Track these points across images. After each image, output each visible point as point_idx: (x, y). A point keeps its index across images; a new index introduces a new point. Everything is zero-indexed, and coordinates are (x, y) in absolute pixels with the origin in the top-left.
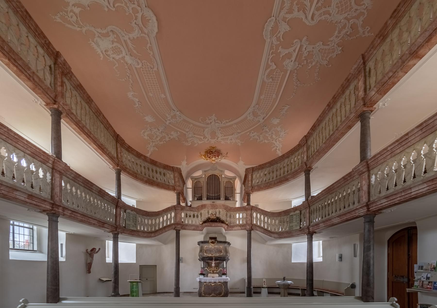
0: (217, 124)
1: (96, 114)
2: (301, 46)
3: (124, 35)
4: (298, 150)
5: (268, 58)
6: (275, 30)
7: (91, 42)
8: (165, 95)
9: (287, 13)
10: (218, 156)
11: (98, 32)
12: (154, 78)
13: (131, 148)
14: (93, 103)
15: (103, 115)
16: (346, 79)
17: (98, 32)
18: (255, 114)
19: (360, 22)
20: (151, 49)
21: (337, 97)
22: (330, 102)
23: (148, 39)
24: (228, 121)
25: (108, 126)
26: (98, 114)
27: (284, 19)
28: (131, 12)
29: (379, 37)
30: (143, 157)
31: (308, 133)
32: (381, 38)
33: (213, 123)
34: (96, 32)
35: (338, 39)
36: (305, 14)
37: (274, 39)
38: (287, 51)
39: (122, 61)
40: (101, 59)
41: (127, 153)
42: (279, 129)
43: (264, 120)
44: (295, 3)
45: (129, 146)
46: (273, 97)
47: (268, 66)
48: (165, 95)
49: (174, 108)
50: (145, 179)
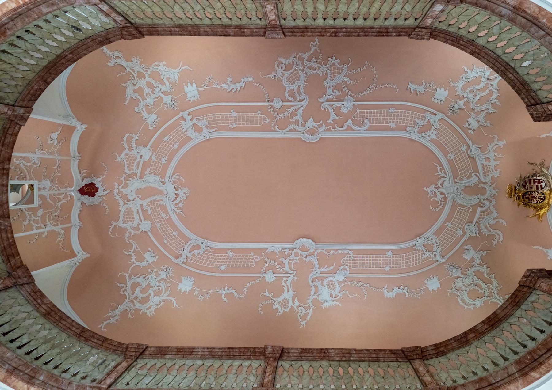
0: (446, 184)
1: (344, 359)
2: (328, 101)
3: (316, 272)
4: (446, 32)
5: (339, 131)
6: (312, 132)
7: (323, 306)
8: (388, 251)
9: (298, 125)
10: (539, 182)
11: (314, 295)
12: (209, 264)
13: (441, 343)
14: (331, 351)
15: (355, 350)
16: (294, 36)
17: (314, 295)
18: (424, 130)
19: (305, 56)
20: (328, 251)
21: (317, 31)
22: (331, 36)
23: (320, 251)
24: (439, 168)
25: (374, 355)
26: (348, 355)
27: (303, 125)
28: (297, 258)
29: (244, 32)
30: (472, 335)
31: (400, 35)
32: (242, 30)
33: (443, 191)
34: (314, 297)
35: (321, 66)
36: (299, 108)
37: (320, 130)
38: (332, 114)
39: (343, 285)
40: (340, 305)
41: (442, 359)
42: (460, 84)
43: (437, 113)
44: (291, 120)
45: (435, 345)
46: (393, 111)
47: (350, 129)
48: (388, 251)
49: (411, 244)
50: (513, 369)
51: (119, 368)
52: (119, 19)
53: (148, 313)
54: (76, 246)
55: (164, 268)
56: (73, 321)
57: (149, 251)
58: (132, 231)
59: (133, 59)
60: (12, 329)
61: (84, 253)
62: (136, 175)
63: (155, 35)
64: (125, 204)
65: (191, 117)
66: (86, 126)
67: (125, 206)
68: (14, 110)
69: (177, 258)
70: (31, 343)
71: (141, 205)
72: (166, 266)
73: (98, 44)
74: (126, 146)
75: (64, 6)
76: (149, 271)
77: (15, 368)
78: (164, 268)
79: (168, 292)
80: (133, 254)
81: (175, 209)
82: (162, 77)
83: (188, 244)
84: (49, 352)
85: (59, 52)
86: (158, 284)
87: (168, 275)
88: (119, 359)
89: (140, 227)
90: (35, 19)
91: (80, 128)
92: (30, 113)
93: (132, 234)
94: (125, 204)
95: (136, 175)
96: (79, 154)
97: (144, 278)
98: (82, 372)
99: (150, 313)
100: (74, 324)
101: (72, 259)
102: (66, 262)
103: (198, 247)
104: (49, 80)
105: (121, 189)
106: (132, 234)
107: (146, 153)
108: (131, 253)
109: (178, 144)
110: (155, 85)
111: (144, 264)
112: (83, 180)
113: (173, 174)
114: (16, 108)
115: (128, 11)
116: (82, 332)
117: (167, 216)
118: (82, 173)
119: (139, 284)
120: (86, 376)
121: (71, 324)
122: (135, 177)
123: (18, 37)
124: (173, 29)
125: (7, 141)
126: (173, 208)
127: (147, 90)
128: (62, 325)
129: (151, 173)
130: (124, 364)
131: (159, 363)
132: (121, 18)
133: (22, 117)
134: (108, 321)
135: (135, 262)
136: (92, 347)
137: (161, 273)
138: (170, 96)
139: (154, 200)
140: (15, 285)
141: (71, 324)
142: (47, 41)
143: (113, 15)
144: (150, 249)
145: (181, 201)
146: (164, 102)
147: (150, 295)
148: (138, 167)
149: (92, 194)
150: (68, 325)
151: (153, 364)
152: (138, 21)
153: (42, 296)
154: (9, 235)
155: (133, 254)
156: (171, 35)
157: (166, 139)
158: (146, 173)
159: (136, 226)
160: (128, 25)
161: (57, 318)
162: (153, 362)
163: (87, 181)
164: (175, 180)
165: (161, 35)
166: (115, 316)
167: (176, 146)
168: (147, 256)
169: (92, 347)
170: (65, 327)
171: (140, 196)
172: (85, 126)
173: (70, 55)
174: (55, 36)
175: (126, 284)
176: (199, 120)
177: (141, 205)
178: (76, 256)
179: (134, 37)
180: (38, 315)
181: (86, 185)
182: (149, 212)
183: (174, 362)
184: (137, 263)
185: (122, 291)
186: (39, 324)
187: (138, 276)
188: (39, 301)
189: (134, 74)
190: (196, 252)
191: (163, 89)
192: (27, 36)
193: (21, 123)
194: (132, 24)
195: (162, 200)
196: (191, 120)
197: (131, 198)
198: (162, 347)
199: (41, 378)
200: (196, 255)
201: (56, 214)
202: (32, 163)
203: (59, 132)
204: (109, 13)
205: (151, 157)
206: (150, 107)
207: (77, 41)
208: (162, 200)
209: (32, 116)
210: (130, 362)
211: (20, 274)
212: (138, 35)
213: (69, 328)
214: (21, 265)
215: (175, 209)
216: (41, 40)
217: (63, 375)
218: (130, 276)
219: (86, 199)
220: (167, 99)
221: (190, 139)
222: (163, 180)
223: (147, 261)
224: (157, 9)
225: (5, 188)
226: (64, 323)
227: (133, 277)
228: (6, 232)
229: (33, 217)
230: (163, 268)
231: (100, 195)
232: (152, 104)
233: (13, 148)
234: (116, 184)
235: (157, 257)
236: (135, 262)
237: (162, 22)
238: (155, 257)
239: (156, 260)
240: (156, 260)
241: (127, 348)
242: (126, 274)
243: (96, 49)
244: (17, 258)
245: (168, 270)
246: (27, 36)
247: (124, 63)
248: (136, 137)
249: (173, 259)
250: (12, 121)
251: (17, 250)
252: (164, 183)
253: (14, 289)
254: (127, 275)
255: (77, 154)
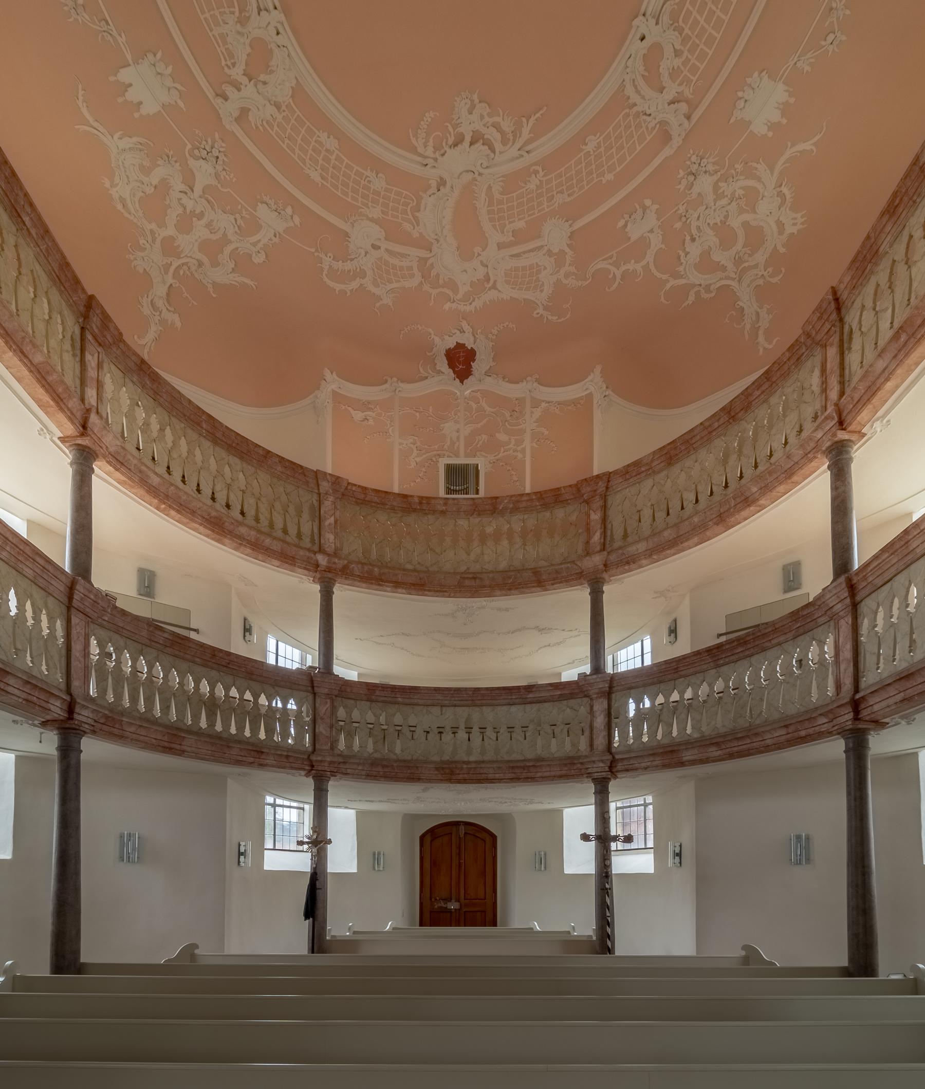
51: (829, 366)
52: (91, 360)
53: (794, 230)
54: (573, 392)
55: (684, 182)
56: (701, 424)
57: (626, 225)
58: (563, 271)
59: (141, 271)
60: (666, 509)
61: (590, 378)
62: (423, 261)
63: (73, 272)
64: (494, 287)
65: (229, 90)
66: (327, 373)
67: (499, 286)
68: (326, 494)
69: (666, 137)
70: (700, 489)
71: (500, 246)
72: (682, 173)
73: (160, 383)
74: (354, 285)
75: (134, 457)
76: (678, 225)
77: (720, 516)
78: (684, 182)
79: (762, 168)
80: (624, 268)
81: (518, 144)
82: (150, 190)
83: (635, 98)
84: (727, 471)
85: (207, 444)
86: (724, 202)
87: (711, 168)
88: (817, 360)
89: (555, 250)
90: (177, 487)
91: (332, 383)
92: (325, 474)
93: (573, 269)
94: (494, 287)
95: (423, 261)
96: (386, 382)
97: (693, 240)
98: (788, 432)
99: (794, 222)
100: (707, 424)
101: (595, 402)
102: (597, 415)
103: (653, 57)
104: (261, 452)
105: (460, 296)
106: (573, 269)
107: (364, 234)
108: (618, 274)
109: (323, 136)
110: (180, 211)
111: (656, 242)
112: (440, 372)
113: (414, 150)
114: (321, 491)
115: (67, 351)
116: (729, 412)
117: (536, 173)
118: (426, 375)
119: (706, 254)
120: (801, 426)
121: (706, 428)
122: (430, 262)
123: (213, 499)
124: (33, 232)
125: (376, 499)
126: (513, 151)
127: (200, 231)
128: (699, 443)
129: (417, 219)
130: (832, 352)
131: (881, 276)
132: (88, 357)
133: (333, 483)
134: (761, 332)
135: (643, 263)
136: (766, 401)
137: (696, 190)
138: (192, 163)
139: (489, 212)
140: (604, 498)
141: (706, 428)
142: (200, 464)
143: (92, 373)
144: (621, 223)
145: (496, 126)
146: (214, 182)
147: (746, 225)
148: (402, 255)
149: (471, 355)
150: (706, 432)
151: (872, 292)
152: (70, 320)
153: (637, 464)
154: (525, 498)
155: (624, 268)
156: (47, 231)
157: (315, 175)
158: (416, 235)
159: (552, 259)
160: (90, 337)
161: (683, 448)
162: (870, 289)
163: (443, 364)
164: (431, 144)
165: (64, 257)
166: (758, 314)
167: (331, 143)
168: (635, 231)
169: (764, 402)
170: (705, 439)
171: (477, 249)
172: (328, 375)
173: (204, 426)
174: (185, 454)
175: (694, 286)
176: (232, 56)
177: (500, 246)
178: (590, 396)
179: (106, 318)
180: (664, 473)
181: (451, 365)
182: (521, 224)
183: (905, 238)
184: (650, 258)
185: (705, 296)
186: (680, 474)
187: (682, 254)
188: (643, 469)
189: (175, 265)
190: (665, 66)
191: (178, 185)
192: (207, 491)
193: (345, 484)
194: (83, 329)
195: (490, 188)
196: (238, 87)
197: (481, 272)
198: (859, 252)
199: (754, 489)
200: (677, 62)
201: (507, 415)
202: (414, 448)
203: (350, 409)
204: (95, 383)
205: (372, 220)
206: (239, 221)
207: (173, 419)
208: (490, 188)
209: (329, 471)
210: (836, 339)
211: (589, 489)
212: (98, 312)
213: (710, 433)
214: (577, 487)
215: (518, 144)
216: (202, 472)
217: (773, 460)
218: (676, 276)
219: (478, 367)
220: (204, 173)
221: (298, 91)
222: (434, 184)
223: (651, 231)
224: (26, 293)
225: (450, 502)
226: (698, 437)
227: (681, 269)
228: (518, 502)
229: (510, 446)
230: (682, 187)
231: (472, 339)
232: (232, 218)
233: (386, 492)
234: (447, 306)
235: (648, 202)
236: (643, 263)
237: (38, 267)
238: (645, 209)
239: (656, 207)
240: (656, 207)
241: (808, 335)
242: (668, 286)
243: (169, 384)
244: (563, 491)
245: (694, 168)
246: (207, 491)
247: (160, 290)
248: (327, 261)
249: (667, 152)
250: (343, 495)
251: (551, 490)
252: (442, 183)
253: (610, 499)
254: (672, 283)
255: (386, 386)
